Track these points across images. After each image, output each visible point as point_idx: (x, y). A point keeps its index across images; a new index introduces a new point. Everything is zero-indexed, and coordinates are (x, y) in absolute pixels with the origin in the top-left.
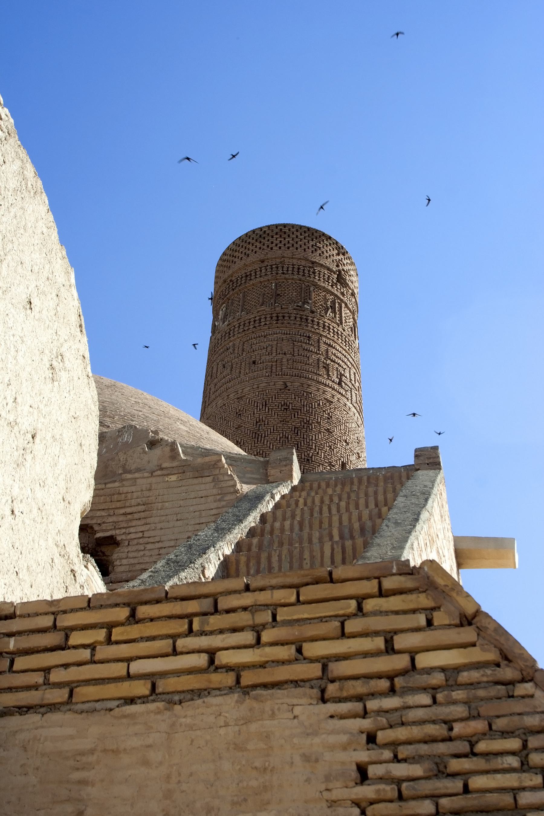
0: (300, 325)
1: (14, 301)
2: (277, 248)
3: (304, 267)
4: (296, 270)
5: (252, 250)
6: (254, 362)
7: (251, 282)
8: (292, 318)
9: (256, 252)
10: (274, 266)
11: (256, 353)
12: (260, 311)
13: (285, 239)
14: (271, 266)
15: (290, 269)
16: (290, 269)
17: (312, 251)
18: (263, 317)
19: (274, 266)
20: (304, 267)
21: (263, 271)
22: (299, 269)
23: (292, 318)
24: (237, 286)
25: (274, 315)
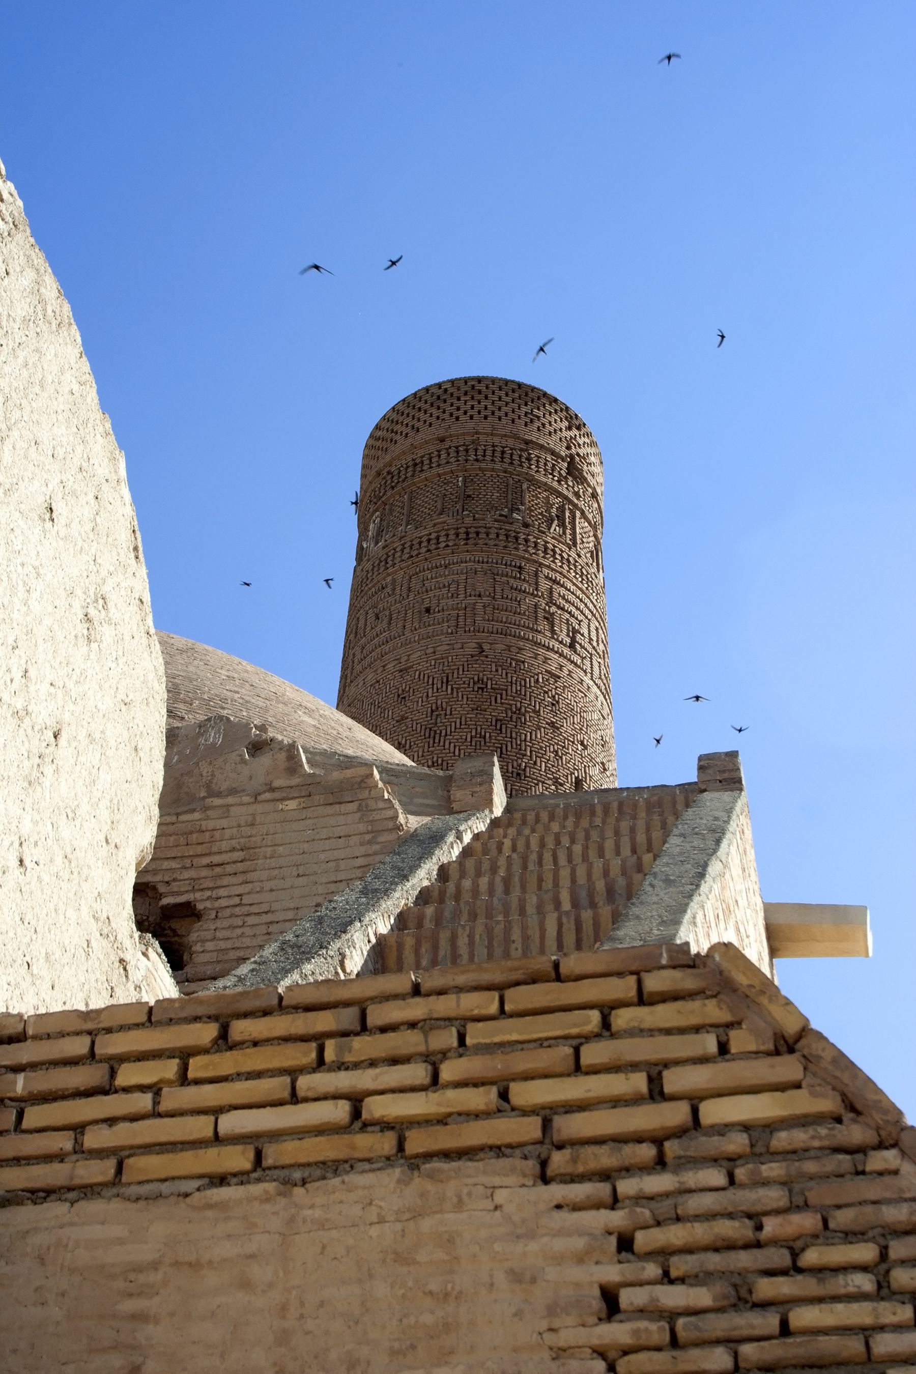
0: (505, 547)
1: (23, 507)
2: (467, 417)
3: (511, 449)
4: (498, 454)
5: (425, 421)
6: (428, 610)
7: (423, 476)
8: (492, 536)
9: (430, 425)
10: (461, 449)
11: (431, 594)
12: (438, 523)
13: (479, 402)
14: (457, 447)
15: (489, 453)
16: (489, 453)
17: (526, 423)
18: (443, 533)
19: (461, 449)
20: (511, 449)
21: (443, 456)
22: (503, 452)
23: (492, 536)
24: (398, 482)
25: (462, 530)
